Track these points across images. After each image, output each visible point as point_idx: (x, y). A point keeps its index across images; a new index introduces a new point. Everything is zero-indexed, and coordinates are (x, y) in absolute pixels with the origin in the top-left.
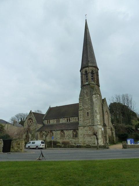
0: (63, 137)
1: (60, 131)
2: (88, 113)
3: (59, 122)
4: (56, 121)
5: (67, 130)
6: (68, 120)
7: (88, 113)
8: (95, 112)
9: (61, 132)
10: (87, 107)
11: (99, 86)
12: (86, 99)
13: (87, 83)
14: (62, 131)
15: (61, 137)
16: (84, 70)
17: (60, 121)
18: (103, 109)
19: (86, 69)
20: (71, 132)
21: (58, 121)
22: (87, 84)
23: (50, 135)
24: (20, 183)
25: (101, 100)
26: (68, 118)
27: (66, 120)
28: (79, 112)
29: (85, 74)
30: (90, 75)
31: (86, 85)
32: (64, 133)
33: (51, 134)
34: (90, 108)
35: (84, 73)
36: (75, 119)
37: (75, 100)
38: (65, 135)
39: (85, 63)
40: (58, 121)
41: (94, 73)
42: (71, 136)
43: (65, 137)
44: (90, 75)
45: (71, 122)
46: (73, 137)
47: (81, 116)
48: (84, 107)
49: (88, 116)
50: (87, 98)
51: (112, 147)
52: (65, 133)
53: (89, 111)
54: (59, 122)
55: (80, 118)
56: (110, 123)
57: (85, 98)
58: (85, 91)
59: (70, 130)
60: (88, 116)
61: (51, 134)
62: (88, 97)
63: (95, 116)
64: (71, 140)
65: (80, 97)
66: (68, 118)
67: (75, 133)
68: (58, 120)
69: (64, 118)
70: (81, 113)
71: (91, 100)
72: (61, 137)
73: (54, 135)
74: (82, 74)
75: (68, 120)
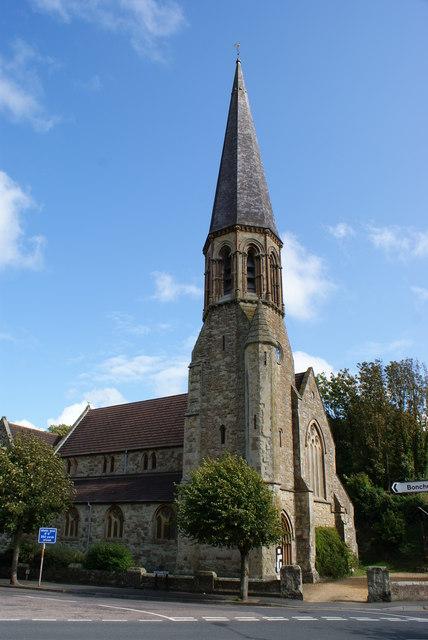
0: (71, 534)
1: (107, 507)
2: (223, 429)
3: (112, 470)
4: (101, 466)
5: (132, 503)
6: (150, 463)
7: (223, 429)
8: (252, 426)
9: (111, 510)
10: (219, 400)
11: (283, 315)
12: (218, 369)
13: (227, 298)
14: (115, 507)
15: (109, 535)
16: (218, 244)
17: (117, 464)
18: (295, 417)
19: (224, 238)
20: (148, 513)
21: (109, 465)
22: (226, 303)
23: (67, 525)
24: (410, 402)
25: (292, 381)
26: (151, 452)
27: (141, 464)
28: (187, 424)
29: (220, 261)
30: (241, 265)
31: (243, 563)
32: (122, 519)
33: (71, 519)
34: (232, 407)
35: (216, 256)
36: (176, 455)
37: (172, 379)
38: (126, 528)
39: (221, 218)
40: (109, 465)
41: (259, 258)
42: (150, 534)
43: (125, 536)
44: (241, 265)
45: (159, 469)
46: (159, 536)
47: (194, 444)
48: (208, 401)
49: (223, 442)
50: (221, 362)
51: (321, 593)
52: (127, 515)
53: (230, 418)
54: (112, 470)
55: (190, 451)
56: (333, 481)
57: (215, 365)
58: (215, 332)
59: (148, 503)
60: (223, 442)
61: (71, 519)
62: (228, 359)
63: (251, 441)
64: (146, 548)
65: (194, 358)
66: (151, 452)
67: (165, 520)
68: (109, 460)
69: (134, 451)
70: (193, 430)
71: (238, 370)
72: (109, 535)
73: (82, 523)
74: (209, 262)
75: (150, 463)
